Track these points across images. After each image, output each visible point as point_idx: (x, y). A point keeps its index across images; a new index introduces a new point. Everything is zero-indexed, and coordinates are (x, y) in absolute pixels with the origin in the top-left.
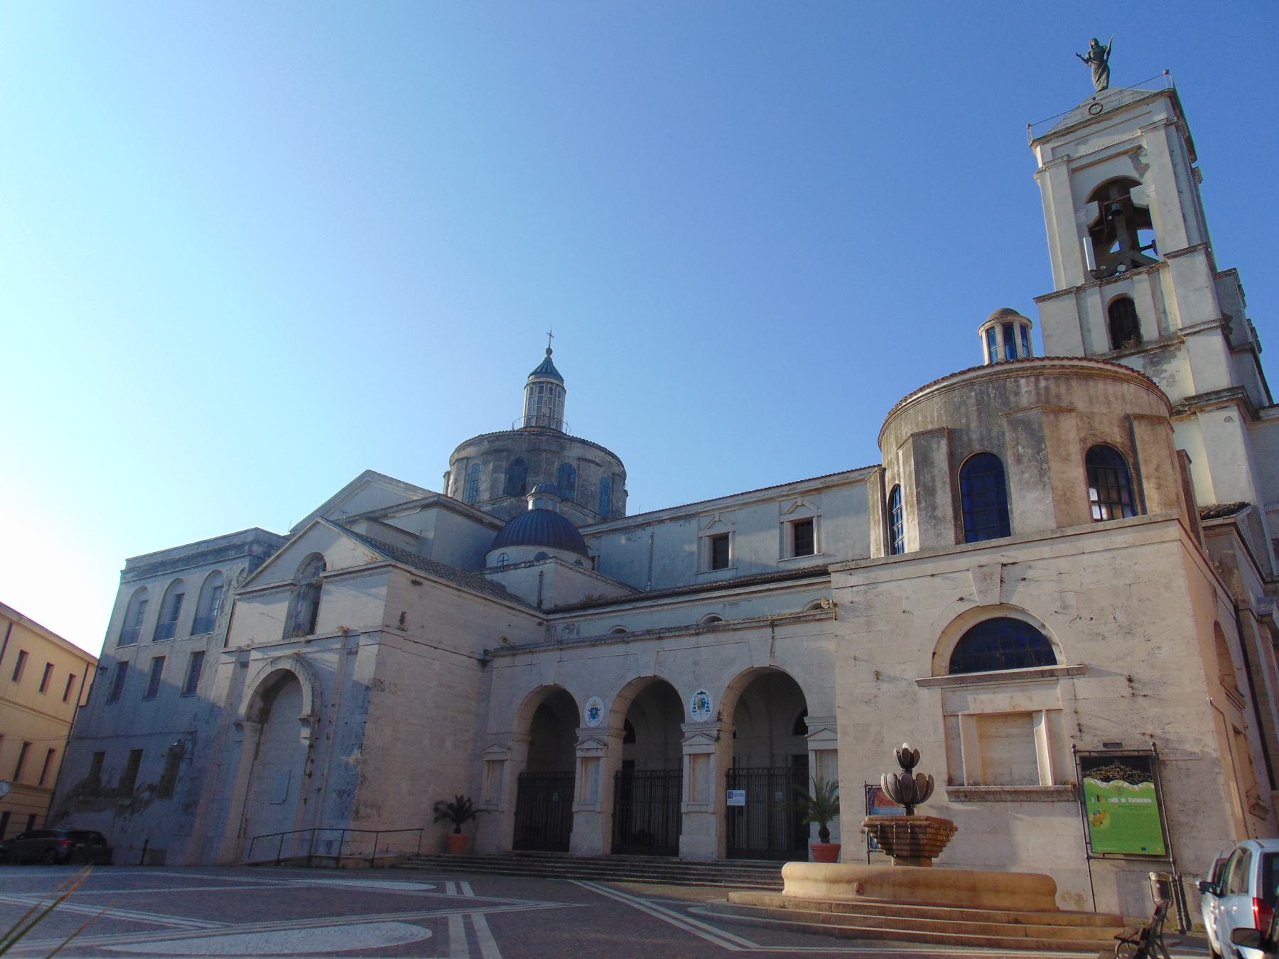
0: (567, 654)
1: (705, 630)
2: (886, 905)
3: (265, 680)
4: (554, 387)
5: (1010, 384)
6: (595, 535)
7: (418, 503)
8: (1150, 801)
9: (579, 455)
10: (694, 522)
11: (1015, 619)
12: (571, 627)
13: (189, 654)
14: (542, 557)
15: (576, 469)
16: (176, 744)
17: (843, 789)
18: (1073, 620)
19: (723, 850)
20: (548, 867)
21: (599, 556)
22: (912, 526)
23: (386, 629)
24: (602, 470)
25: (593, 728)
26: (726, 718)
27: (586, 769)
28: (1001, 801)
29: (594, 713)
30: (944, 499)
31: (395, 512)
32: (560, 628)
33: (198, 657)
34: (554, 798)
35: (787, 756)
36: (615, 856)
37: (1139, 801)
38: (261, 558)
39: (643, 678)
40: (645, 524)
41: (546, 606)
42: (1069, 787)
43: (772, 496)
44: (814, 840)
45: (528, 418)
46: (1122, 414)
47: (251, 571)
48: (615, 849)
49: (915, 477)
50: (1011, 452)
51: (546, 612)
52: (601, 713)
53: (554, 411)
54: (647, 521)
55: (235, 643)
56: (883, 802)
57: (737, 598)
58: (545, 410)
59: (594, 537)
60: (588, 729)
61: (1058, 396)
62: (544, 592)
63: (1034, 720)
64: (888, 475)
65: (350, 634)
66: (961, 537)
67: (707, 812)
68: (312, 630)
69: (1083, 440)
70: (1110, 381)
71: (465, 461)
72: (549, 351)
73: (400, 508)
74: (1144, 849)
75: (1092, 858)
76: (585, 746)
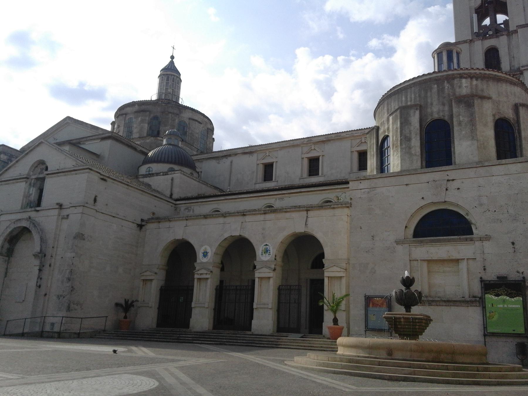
0: (190, 223)
1: (269, 211)
2: (412, 362)
4: (175, 77)
5: (456, 81)
7: (100, 137)
9: (190, 117)
10: (255, 155)
12: (189, 208)
14: (172, 170)
15: (188, 123)
17: (352, 297)
18: (485, 212)
19: (276, 328)
21: (201, 172)
22: (396, 158)
23: (86, 205)
24: (202, 126)
25: (204, 263)
26: (279, 259)
27: (200, 285)
28: (440, 306)
29: (205, 254)
30: (416, 143)
31: (85, 141)
32: (182, 209)
34: (181, 300)
35: (307, 280)
36: (215, 331)
39: (233, 236)
41: (175, 196)
42: (478, 299)
45: (160, 94)
46: (514, 103)
48: (214, 328)
50: (456, 119)
52: (209, 255)
53: (175, 91)
54: (229, 154)
57: (283, 196)
58: (170, 90)
59: (199, 161)
60: (202, 263)
61: (482, 90)
62: (174, 189)
63: (460, 264)
64: (381, 131)
65: (63, 207)
66: (424, 164)
68: (39, 204)
69: (494, 115)
70: (508, 84)
72: (172, 57)
73: (88, 138)
75: (487, 335)
76: (199, 272)
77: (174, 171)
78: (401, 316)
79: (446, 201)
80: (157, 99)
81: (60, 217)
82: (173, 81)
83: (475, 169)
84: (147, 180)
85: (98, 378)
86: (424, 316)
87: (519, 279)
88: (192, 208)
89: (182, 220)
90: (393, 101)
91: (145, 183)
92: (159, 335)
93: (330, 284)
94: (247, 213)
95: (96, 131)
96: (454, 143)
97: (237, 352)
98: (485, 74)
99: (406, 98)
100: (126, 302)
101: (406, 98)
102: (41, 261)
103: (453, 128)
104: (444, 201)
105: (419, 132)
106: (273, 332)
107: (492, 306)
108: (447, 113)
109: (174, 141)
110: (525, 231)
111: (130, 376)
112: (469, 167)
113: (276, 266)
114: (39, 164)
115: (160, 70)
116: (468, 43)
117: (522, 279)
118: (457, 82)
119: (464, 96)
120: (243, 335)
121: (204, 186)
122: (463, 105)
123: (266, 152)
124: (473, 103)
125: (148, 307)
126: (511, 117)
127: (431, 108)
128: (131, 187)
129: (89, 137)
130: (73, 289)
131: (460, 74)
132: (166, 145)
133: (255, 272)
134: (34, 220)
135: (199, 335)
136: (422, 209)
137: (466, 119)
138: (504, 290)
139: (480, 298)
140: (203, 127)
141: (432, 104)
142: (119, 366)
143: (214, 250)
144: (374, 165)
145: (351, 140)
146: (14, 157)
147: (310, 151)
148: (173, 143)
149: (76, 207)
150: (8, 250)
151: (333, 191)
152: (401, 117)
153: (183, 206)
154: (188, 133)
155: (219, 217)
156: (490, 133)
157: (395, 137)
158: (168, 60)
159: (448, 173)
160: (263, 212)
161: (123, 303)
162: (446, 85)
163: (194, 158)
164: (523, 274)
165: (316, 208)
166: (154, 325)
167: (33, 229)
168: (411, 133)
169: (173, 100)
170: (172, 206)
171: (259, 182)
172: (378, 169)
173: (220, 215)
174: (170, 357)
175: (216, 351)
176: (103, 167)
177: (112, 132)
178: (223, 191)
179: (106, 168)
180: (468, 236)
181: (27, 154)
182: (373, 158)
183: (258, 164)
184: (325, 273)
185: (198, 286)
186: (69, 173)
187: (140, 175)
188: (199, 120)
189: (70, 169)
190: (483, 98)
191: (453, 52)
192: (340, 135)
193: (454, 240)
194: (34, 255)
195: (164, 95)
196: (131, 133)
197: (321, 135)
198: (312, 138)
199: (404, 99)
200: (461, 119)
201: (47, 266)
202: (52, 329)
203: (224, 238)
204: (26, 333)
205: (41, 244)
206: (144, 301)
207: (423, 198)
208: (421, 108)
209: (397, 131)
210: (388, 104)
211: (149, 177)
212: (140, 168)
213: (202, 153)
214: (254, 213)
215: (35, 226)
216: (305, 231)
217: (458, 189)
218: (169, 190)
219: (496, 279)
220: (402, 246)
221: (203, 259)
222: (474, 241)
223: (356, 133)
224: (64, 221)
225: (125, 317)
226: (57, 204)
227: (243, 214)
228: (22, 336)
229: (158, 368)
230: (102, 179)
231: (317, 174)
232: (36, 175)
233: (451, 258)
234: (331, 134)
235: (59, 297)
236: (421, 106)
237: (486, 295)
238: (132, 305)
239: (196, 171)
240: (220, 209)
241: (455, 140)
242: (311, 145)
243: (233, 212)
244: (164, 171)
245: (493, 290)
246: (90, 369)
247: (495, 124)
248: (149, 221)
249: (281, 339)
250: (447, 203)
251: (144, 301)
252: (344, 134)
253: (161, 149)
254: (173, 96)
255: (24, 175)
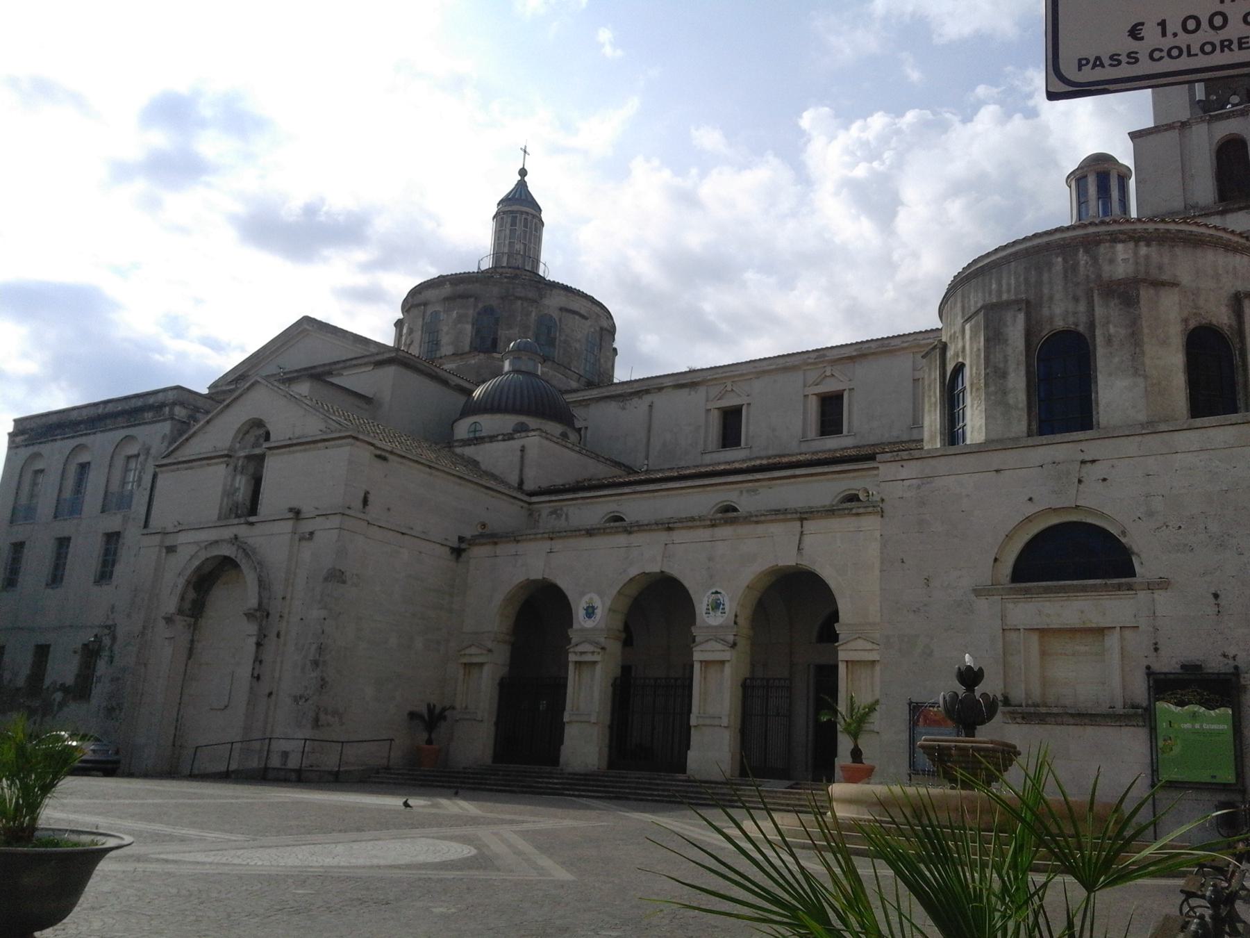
0: (558, 545)
1: (722, 522)
3: (199, 568)
4: (530, 218)
5: (1103, 249)
6: (585, 403)
7: (372, 359)
8: (1226, 727)
10: (702, 391)
11: (1095, 525)
13: (101, 535)
14: (522, 429)
15: (557, 319)
16: (93, 639)
20: (541, 783)
21: (586, 428)
22: (976, 412)
23: (348, 512)
24: (588, 323)
29: (590, 612)
30: (1017, 382)
32: (545, 513)
33: (113, 539)
34: (541, 706)
35: (809, 665)
37: (1215, 727)
38: (184, 422)
39: (648, 574)
40: (642, 391)
41: (529, 485)
43: (796, 363)
44: (843, 758)
45: (497, 255)
46: (1233, 291)
47: (174, 440)
48: (611, 765)
49: (985, 356)
51: (527, 494)
52: (599, 612)
54: (645, 388)
55: (156, 522)
56: (932, 722)
57: (757, 484)
58: (518, 247)
60: (583, 630)
61: (1160, 267)
62: (526, 470)
63: (1106, 638)
65: (302, 516)
66: (1034, 427)
67: (589, 722)
68: (253, 510)
69: (1186, 321)
71: (423, 307)
72: (523, 172)
73: (348, 364)
74: (1214, 777)
76: (580, 649)
77: (525, 431)
78: (953, 744)
79: (1079, 506)
80: (491, 266)
81: (297, 537)
82: (526, 226)
83: (1138, 439)
84: (469, 451)
85: (376, 842)
86: (996, 744)
87: (1228, 671)
88: (565, 509)
89: (542, 539)
90: (972, 291)
91: (465, 457)
92: (496, 777)
93: (850, 676)
94: (676, 525)
95: (364, 347)
96: (1096, 382)
97: (642, 812)
98: (1168, 231)
99: (1000, 284)
100: (431, 709)
101: (1000, 284)
102: (261, 625)
103: (1095, 349)
104: (1074, 506)
105: (1024, 359)
106: (732, 776)
107: (1171, 726)
108: (1083, 319)
109: (527, 365)
110: (1241, 570)
111: (430, 841)
112: (1127, 433)
113: (737, 637)
114: (251, 428)
115: (498, 202)
116: (1177, 130)
117: (1232, 670)
118: (1105, 250)
119: (1120, 282)
120: (669, 780)
121: (591, 461)
122: (1116, 301)
123: (725, 383)
124: (1138, 296)
125: (475, 720)
126: (1225, 322)
127: (1050, 307)
128: (437, 469)
129: (351, 359)
130: (323, 684)
131: (1111, 234)
132: (509, 372)
133: (694, 649)
134: (246, 543)
135: (577, 779)
136: (1031, 521)
137: (1122, 332)
138: (1195, 693)
139: (1146, 709)
140: (590, 326)
141: (1051, 298)
142: (414, 826)
143: (608, 603)
144: (936, 426)
145: (913, 353)
146: (201, 412)
147: (821, 381)
148: (523, 368)
149: (328, 516)
150: (194, 602)
151: (864, 473)
152: (986, 327)
153: (544, 505)
154: (557, 340)
155: (617, 533)
156: (1175, 359)
157: (974, 369)
158: (513, 180)
159: (1083, 446)
160: (709, 523)
161: (424, 711)
162: (1082, 258)
163: (568, 398)
164: (1235, 660)
165: (820, 514)
166: (488, 760)
167: (244, 561)
168: (1006, 361)
169: (527, 268)
170: (522, 507)
171: (710, 450)
172: (944, 435)
173: (620, 530)
174: (508, 817)
175: (600, 809)
176: (379, 428)
177: (396, 349)
178: (633, 470)
179: (386, 430)
180: (1123, 580)
181: (228, 406)
182: (935, 410)
183: (708, 411)
184: (839, 652)
185: (577, 677)
186: (312, 446)
187: (457, 441)
188: (583, 312)
189: (314, 439)
190: (1158, 284)
191: (1109, 177)
192: (889, 343)
193: (1094, 588)
194: (245, 614)
195: (505, 259)
196: (437, 344)
197: (847, 345)
198: (825, 352)
199: (994, 286)
200: (1112, 330)
201: (273, 636)
202: (285, 763)
203: (628, 579)
204: (232, 772)
205: (259, 593)
206: (466, 708)
207: (1030, 499)
208: (1030, 307)
209: (978, 356)
210: (963, 296)
211: (475, 444)
212: (455, 424)
213: (590, 385)
214: (690, 524)
215: (247, 555)
216: (797, 564)
217: (1104, 480)
218: (517, 472)
219: (1179, 671)
220: (987, 599)
221: (585, 622)
222: (1136, 590)
223: (924, 339)
224: (304, 543)
225: (429, 742)
226: (291, 510)
227: (669, 526)
228: (225, 776)
229: (484, 833)
230: (379, 457)
231: (839, 431)
232: (247, 450)
233: (1089, 625)
234: (867, 341)
235: (296, 699)
236: (1028, 302)
237: (1157, 703)
238: (442, 717)
239: (574, 428)
240: (624, 514)
241: (1100, 377)
242: (825, 367)
243: (646, 522)
244: (505, 432)
245: (1172, 694)
246: (363, 830)
247: (1187, 339)
248: (474, 541)
249: (742, 789)
250: (1081, 509)
251: (466, 708)
252: (898, 342)
253: (499, 384)
254: (525, 259)
255: (222, 450)
